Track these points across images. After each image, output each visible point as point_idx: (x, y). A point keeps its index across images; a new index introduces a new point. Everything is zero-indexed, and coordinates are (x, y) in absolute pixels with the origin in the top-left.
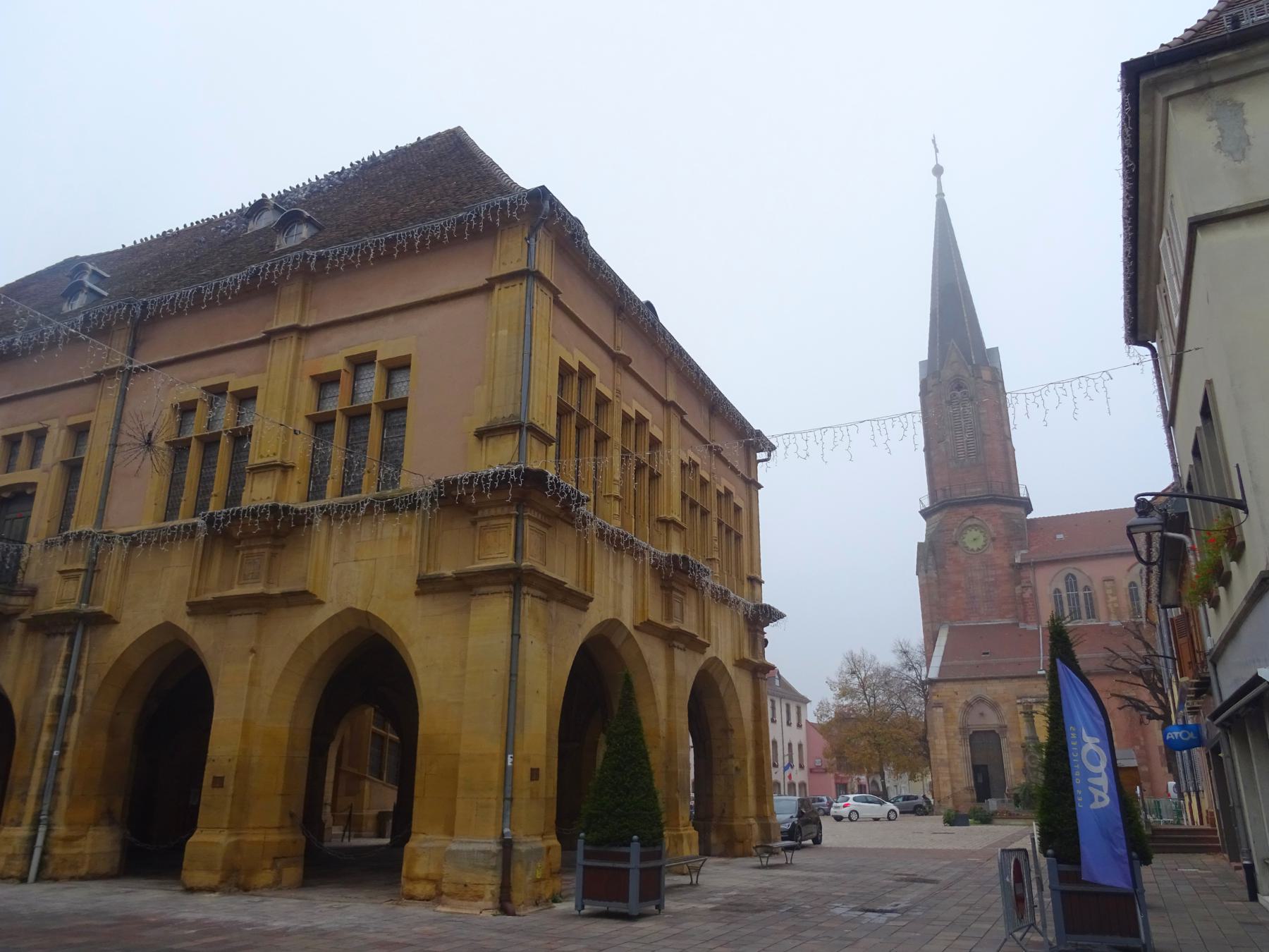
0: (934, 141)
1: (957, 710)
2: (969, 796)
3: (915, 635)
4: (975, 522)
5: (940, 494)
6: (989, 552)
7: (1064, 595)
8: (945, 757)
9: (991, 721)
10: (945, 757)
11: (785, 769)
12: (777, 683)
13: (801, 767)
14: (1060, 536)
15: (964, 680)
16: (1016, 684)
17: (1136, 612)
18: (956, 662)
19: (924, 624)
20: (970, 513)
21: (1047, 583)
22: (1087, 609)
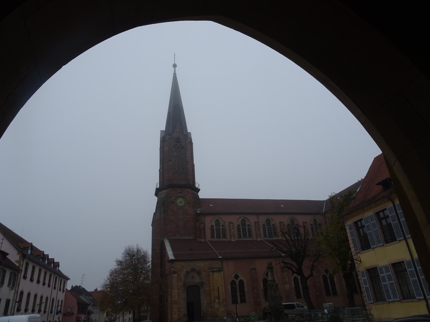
4: (182, 195)
7: (215, 228)
9: (197, 280)
14: (211, 205)
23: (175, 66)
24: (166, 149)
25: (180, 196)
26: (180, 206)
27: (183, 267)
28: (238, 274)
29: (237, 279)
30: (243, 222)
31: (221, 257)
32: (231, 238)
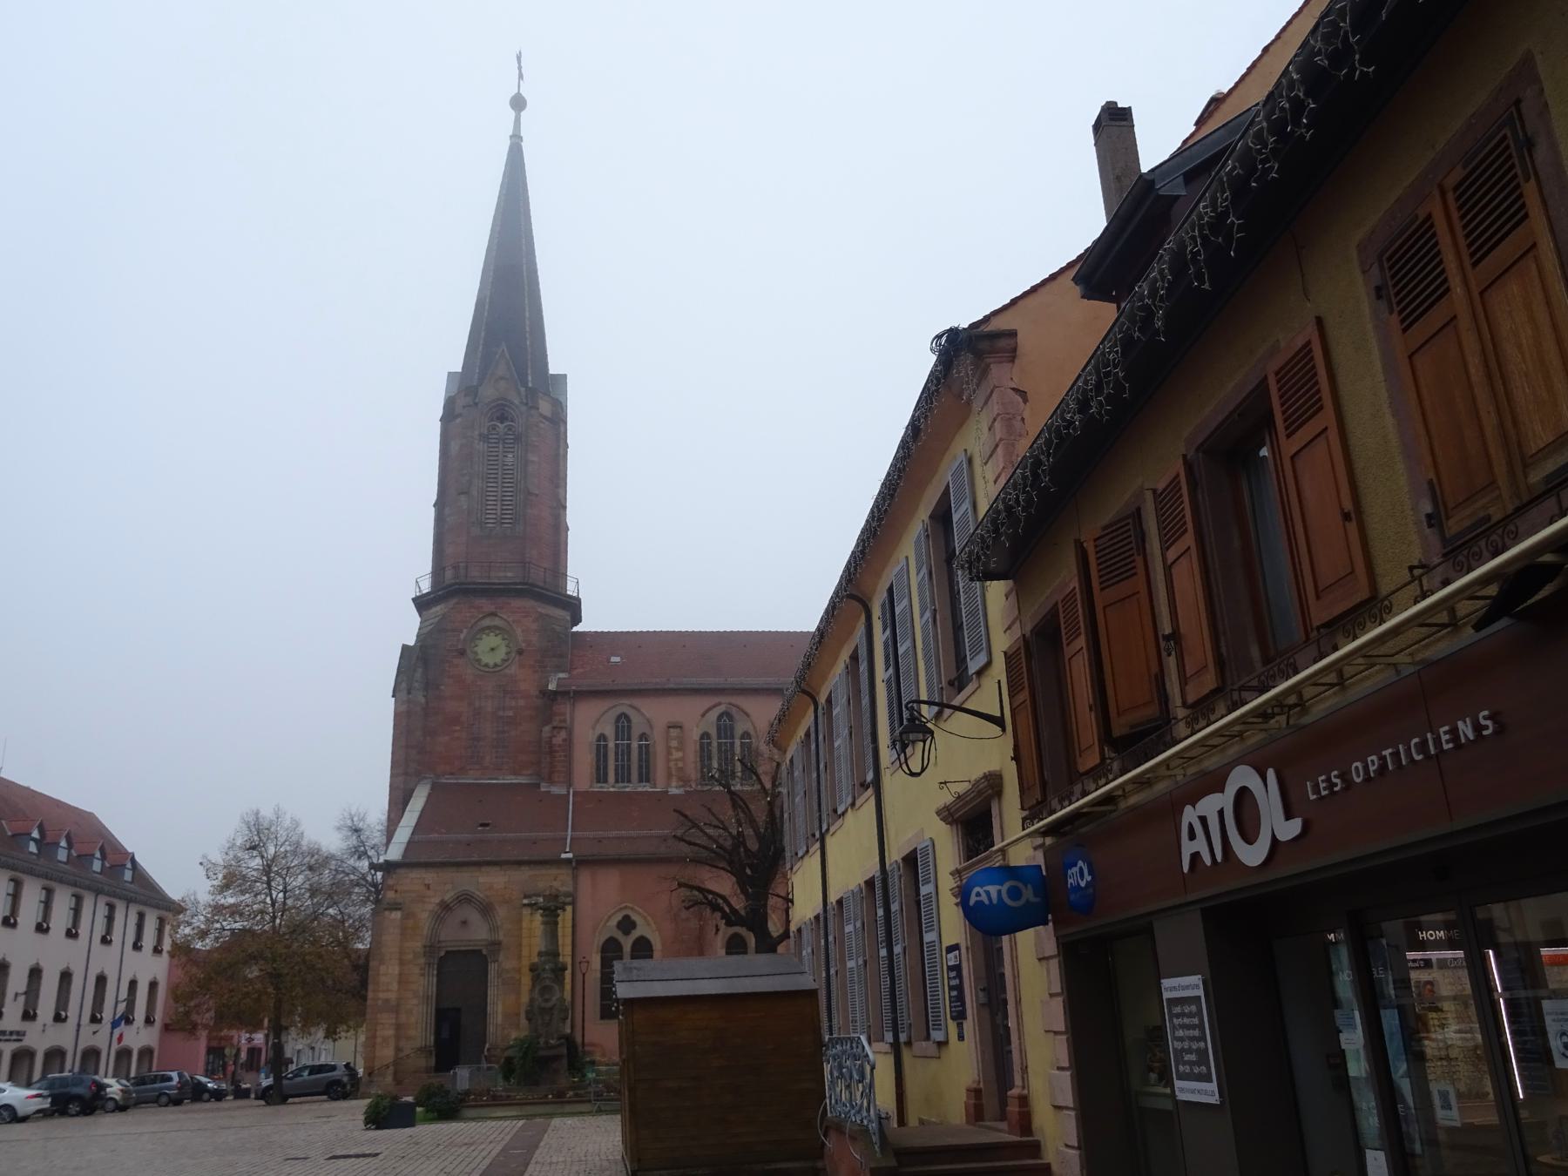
0: (519, 58)
1: (424, 916)
2: (422, 1062)
3: (376, 807)
5: (449, 574)
6: (513, 670)
7: (611, 745)
8: (392, 996)
9: (479, 933)
10: (392, 996)
11: (115, 1024)
12: (128, 875)
13: (149, 1021)
14: (615, 659)
15: (443, 865)
16: (524, 874)
17: (705, 777)
18: (434, 836)
19: (392, 776)
20: (492, 608)
21: (589, 724)
22: (640, 767)
23: (518, 103)
24: (454, 447)
25: (489, 628)
26: (486, 665)
27: (428, 887)
28: (634, 917)
29: (627, 933)
30: (725, 725)
31: (570, 855)
32: (669, 785)
